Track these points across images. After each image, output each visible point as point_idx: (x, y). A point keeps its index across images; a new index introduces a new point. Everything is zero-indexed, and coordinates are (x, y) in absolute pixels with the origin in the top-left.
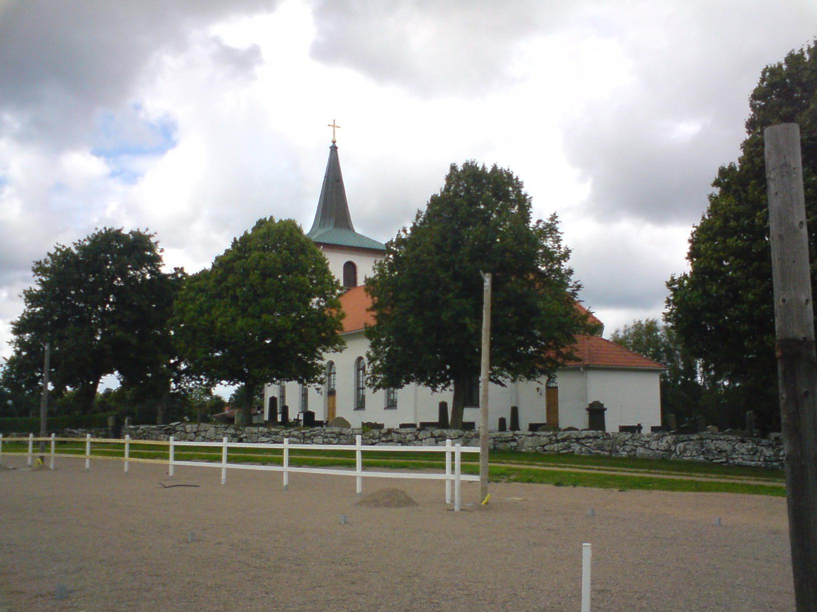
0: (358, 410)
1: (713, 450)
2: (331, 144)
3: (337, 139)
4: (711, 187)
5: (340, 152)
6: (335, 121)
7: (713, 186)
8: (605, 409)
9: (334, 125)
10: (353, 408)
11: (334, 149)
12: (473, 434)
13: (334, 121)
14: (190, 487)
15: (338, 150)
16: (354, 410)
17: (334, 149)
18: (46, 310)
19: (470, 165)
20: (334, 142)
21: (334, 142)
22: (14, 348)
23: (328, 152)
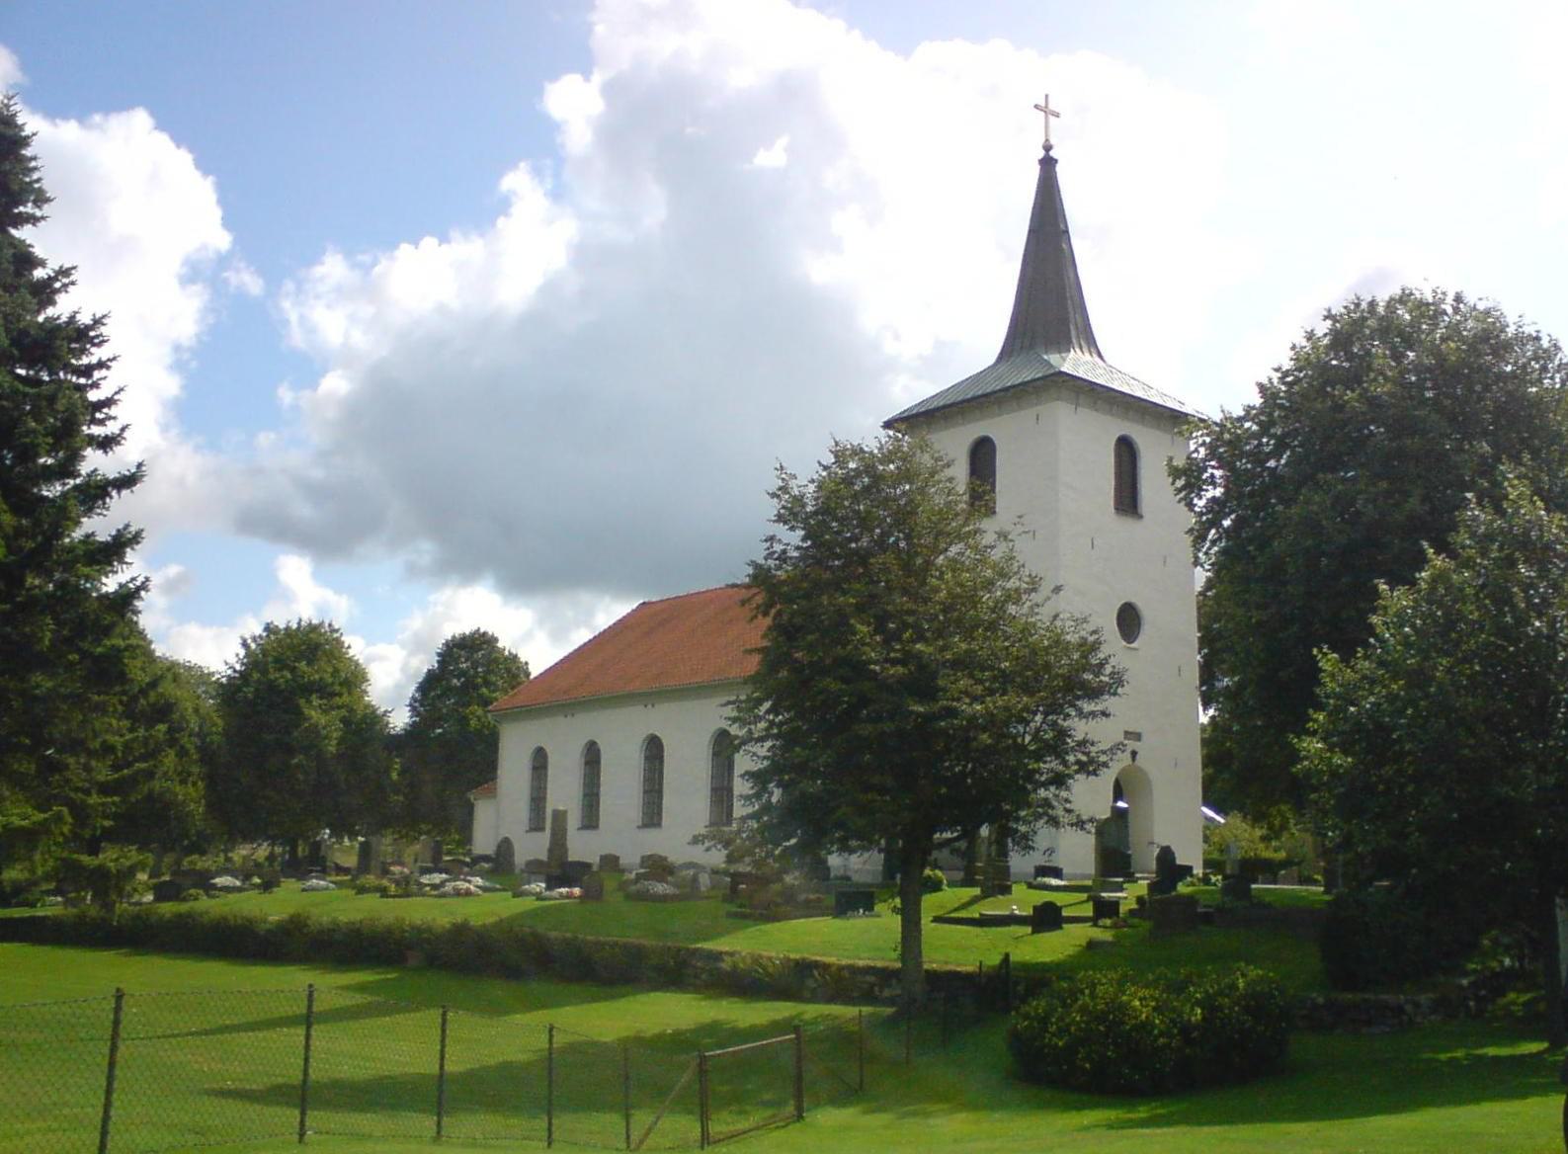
0: (646, 830)
1: (1124, 882)
2: (1041, 154)
3: (1053, 141)
4: (1144, 519)
5: (1062, 172)
6: (1050, 98)
7: (1141, 517)
8: (106, 452)
9: (1046, 107)
10: (637, 824)
11: (1048, 164)
12: (90, 382)
13: (1047, 96)
14: (111, 1128)
15: (1059, 168)
16: (639, 827)
17: (1048, 164)
18: (1544, 637)
19: (1381, 310)
20: (1048, 148)
21: (1048, 148)
22: (1173, 484)
23: (1034, 173)
